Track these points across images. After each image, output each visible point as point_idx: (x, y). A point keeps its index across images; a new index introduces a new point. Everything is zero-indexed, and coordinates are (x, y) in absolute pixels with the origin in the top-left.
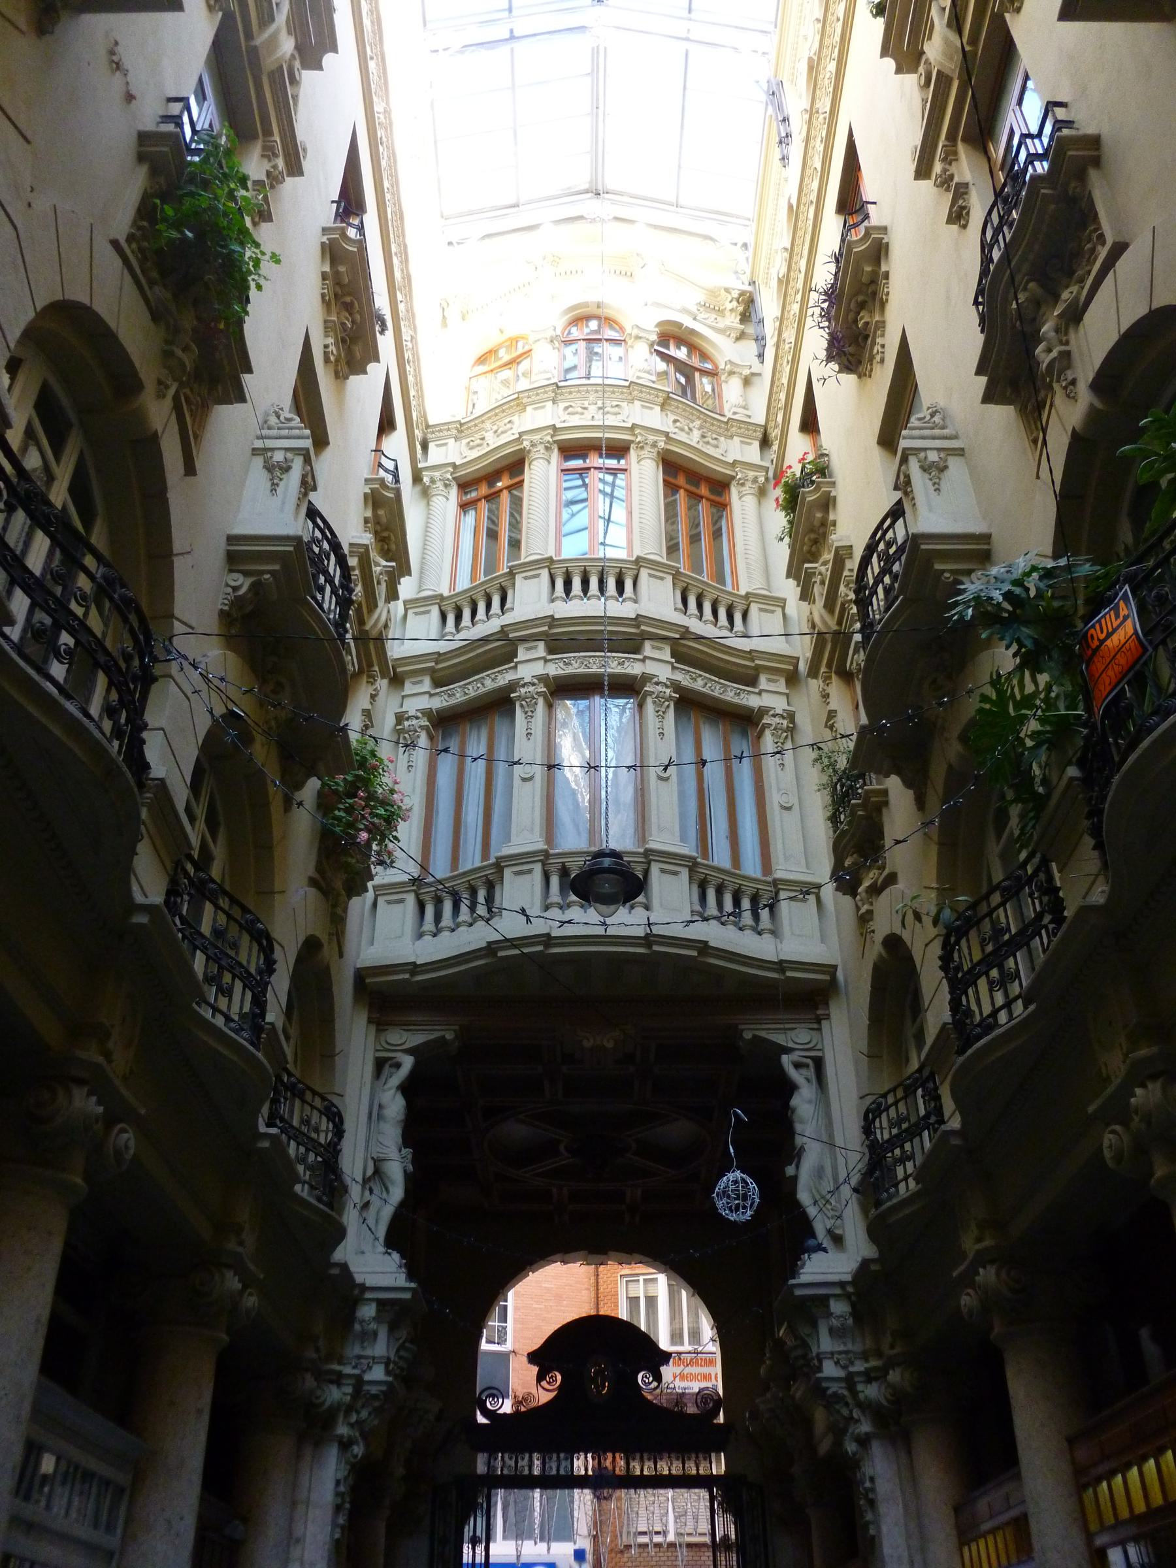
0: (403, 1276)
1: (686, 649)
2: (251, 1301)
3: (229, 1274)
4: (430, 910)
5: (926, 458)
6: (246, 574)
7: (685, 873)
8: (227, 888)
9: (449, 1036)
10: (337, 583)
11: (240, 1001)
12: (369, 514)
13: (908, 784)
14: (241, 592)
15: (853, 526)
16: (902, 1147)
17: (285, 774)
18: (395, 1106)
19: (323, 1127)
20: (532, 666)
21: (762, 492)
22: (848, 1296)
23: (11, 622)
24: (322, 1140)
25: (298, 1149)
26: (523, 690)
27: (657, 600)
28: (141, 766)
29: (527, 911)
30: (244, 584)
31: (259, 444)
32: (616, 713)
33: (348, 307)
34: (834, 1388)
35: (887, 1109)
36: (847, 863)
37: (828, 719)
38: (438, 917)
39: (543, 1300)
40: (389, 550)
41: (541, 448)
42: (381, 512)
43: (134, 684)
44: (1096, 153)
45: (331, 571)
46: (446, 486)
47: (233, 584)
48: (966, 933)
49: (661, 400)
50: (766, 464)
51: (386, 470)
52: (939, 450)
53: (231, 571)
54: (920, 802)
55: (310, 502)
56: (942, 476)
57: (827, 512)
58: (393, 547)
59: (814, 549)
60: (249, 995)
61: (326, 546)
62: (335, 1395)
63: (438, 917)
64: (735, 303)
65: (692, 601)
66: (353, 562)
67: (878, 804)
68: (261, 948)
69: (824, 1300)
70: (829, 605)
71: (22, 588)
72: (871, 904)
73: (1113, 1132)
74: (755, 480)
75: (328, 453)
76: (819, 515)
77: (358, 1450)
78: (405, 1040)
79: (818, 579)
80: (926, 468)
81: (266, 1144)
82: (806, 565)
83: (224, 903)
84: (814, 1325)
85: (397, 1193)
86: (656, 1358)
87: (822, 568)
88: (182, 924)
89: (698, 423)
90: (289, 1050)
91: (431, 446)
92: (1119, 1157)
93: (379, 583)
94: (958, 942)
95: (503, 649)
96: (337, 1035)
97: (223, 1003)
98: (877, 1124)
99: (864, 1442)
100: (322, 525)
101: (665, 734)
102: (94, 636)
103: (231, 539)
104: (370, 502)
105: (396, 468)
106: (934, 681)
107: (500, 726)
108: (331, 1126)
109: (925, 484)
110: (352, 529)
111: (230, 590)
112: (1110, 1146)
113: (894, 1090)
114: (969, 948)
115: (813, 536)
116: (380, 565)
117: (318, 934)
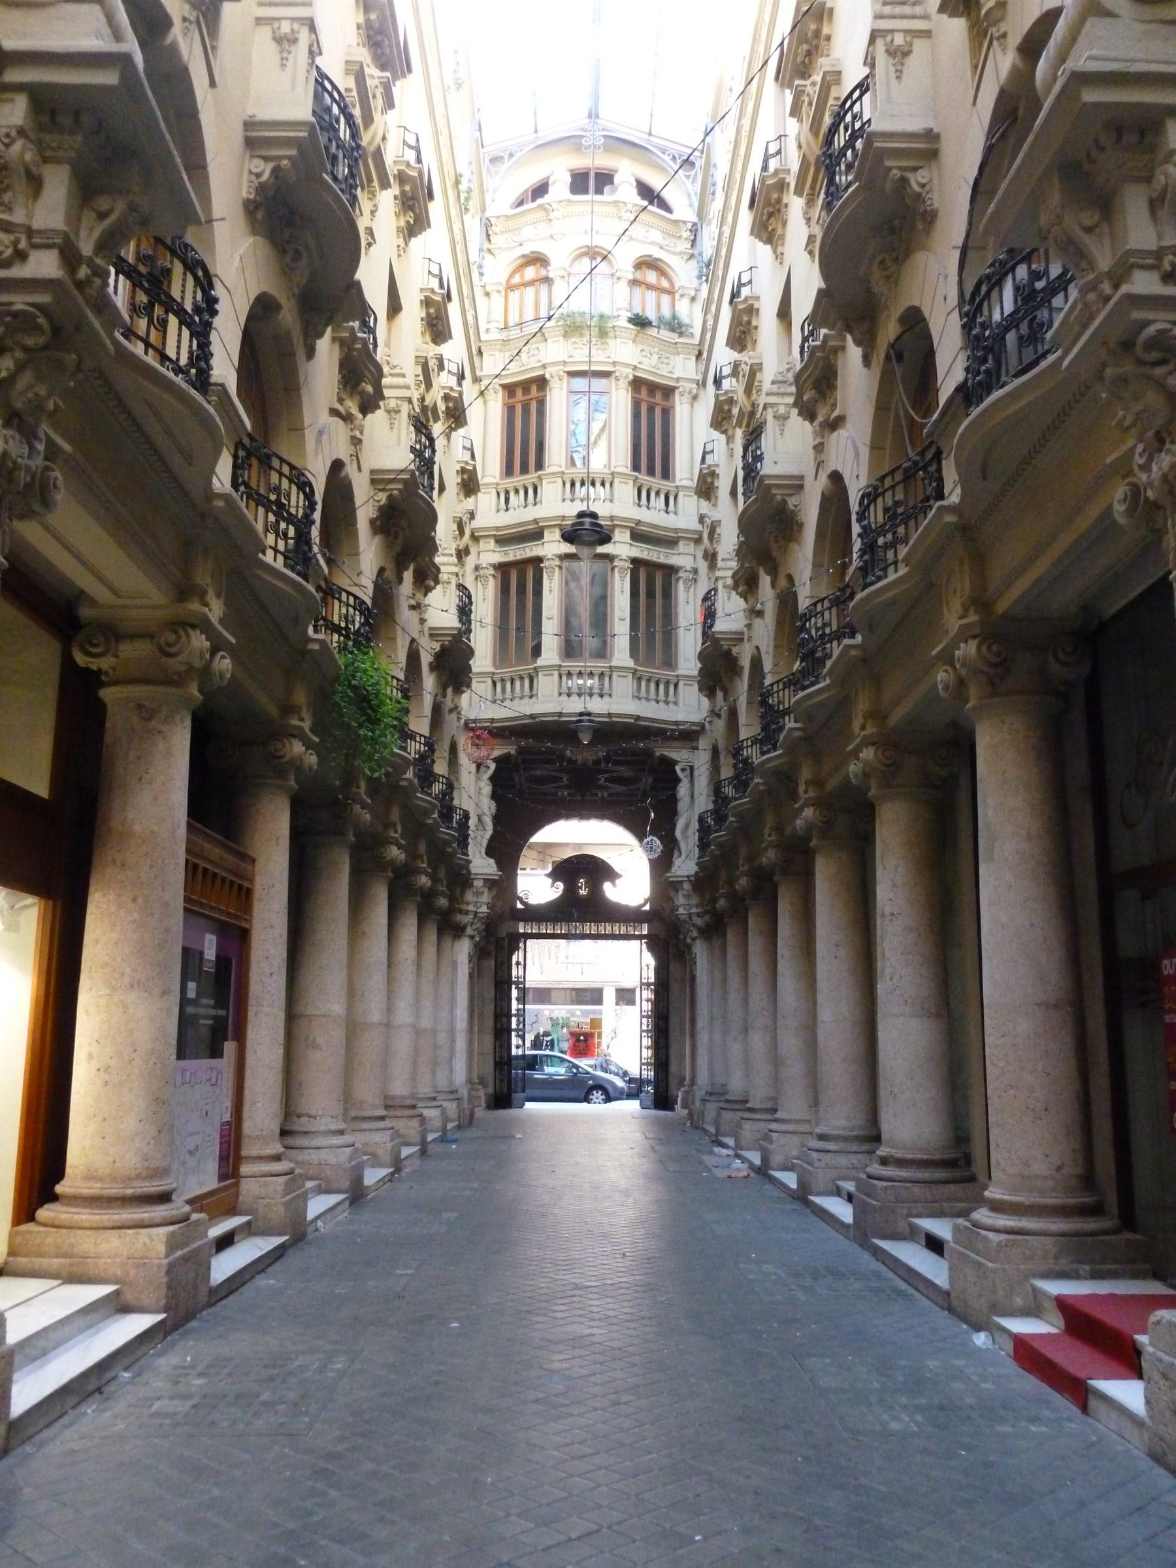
2: (224, 664)
4: (499, 686)
5: (892, 41)
6: (266, 159)
9: (513, 752)
18: (487, 789)
22: (690, 881)
30: (383, 497)
34: (683, 917)
35: (883, 493)
36: (805, 398)
37: (807, 246)
38: (504, 690)
42: (373, 16)
47: (255, 170)
48: (875, 500)
55: (317, 67)
56: (905, 60)
58: (388, 51)
63: (504, 690)
69: (682, 882)
72: (823, 437)
73: (946, 671)
74: (690, 392)
80: (891, 52)
81: (316, 647)
84: (677, 891)
92: (946, 688)
93: (374, 97)
94: (869, 505)
95: (535, 534)
99: (694, 939)
103: (249, 125)
106: (882, 262)
109: (887, 69)
111: (253, 178)
113: (893, 472)
114: (875, 511)
117: (273, 292)
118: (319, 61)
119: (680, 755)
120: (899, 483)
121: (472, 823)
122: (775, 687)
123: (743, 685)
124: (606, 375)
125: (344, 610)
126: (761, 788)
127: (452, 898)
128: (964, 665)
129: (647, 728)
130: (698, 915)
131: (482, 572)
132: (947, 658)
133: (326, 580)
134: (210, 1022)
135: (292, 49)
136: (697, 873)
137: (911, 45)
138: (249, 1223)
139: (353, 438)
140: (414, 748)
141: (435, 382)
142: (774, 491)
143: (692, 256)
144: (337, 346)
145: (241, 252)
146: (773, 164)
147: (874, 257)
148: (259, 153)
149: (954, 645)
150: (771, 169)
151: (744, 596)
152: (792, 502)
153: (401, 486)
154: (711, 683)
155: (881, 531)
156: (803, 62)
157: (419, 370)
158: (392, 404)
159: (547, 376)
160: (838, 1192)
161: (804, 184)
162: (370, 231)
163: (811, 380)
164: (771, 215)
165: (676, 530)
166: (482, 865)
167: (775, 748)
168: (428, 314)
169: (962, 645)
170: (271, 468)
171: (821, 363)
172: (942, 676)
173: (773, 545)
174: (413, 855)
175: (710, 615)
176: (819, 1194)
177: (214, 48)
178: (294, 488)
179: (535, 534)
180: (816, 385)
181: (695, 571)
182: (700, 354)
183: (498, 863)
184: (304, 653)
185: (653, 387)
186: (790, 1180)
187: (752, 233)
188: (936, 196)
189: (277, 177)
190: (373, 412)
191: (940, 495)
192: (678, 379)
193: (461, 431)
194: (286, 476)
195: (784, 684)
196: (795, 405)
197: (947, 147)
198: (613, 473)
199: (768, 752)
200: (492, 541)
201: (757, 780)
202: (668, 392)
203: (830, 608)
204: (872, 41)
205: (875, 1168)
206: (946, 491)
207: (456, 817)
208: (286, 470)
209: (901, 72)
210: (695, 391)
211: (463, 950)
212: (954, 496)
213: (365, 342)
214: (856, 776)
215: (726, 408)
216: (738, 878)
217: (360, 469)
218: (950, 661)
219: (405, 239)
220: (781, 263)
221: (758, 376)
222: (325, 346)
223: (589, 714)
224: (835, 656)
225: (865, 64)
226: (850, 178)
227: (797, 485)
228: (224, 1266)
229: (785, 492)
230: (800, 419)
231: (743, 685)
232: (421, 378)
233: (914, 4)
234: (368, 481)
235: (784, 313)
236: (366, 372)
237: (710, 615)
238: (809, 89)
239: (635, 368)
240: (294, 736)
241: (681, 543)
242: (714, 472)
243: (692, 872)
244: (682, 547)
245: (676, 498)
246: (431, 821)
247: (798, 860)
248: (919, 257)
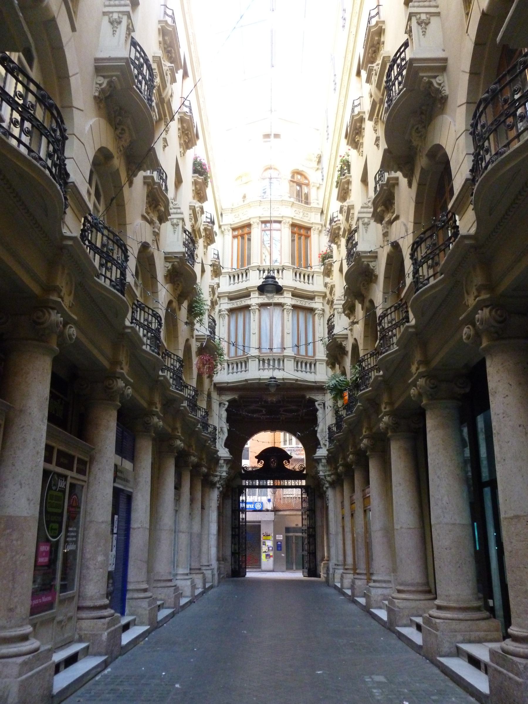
3: (53, 313)
4: (230, 366)
7: (293, 360)
8: (106, 225)
9: (236, 397)
10: (147, 78)
11: (115, 274)
12: (161, 39)
13: (405, 176)
14: (103, 86)
15: (390, 46)
16: (392, 331)
17: (128, 170)
18: (224, 414)
19: (154, 321)
21: (320, 232)
23: (3, 121)
24: (153, 327)
25: (143, 331)
28: (63, 175)
29: (254, 372)
30: (169, 265)
31: (107, 9)
32: (277, 312)
33: (187, 135)
34: (322, 477)
35: (387, 316)
37: (376, 142)
38: (233, 369)
39: (259, 442)
40: (171, 57)
41: (256, 224)
42: (197, 186)
43: (59, 142)
44: (445, 64)
50: (321, 223)
52: (427, 13)
53: (98, 76)
54: (410, 185)
55: (132, 38)
56: (427, 27)
57: (381, 37)
58: (174, 55)
59: (374, 56)
60: (119, 271)
61: (142, 60)
62: (217, 479)
63: (233, 369)
65: (298, 275)
66: (154, 66)
67: (393, 184)
69: (321, 459)
70: (378, 86)
71: (6, 102)
73: (468, 328)
74: (318, 229)
75: (140, 8)
76: (377, 38)
77: (221, 489)
78: (226, 398)
79: (374, 72)
80: (364, 224)
82: (369, 65)
83: (106, 232)
84: (318, 464)
85: (226, 435)
86: (288, 457)
87: (376, 66)
88: (89, 243)
89: (302, 210)
90: (138, 294)
91: (223, 215)
92: (468, 338)
93: (167, 75)
94: (417, 248)
95: (246, 295)
96: (127, 216)
97: (108, 274)
98: (383, 321)
99: (327, 488)
101: (289, 317)
102: (40, 122)
103: (97, 60)
104: (161, 33)
105: (173, 14)
106: (364, 284)
107: (247, 313)
108: (157, 321)
110: (152, 47)
111: (98, 86)
112: (466, 333)
113: (390, 308)
115: (373, 49)
116: (167, 65)
118: (133, 34)
119: (318, 397)
122: (366, 356)
123: (348, 361)
124: (280, 222)
126: (361, 408)
127: (209, 469)
128: (482, 324)
129: (301, 385)
130: (329, 475)
131: (222, 313)
132: (470, 321)
133: (166, 350)
135: (119, 26)
136: (328, 455)
137: (430, 19)
138: (87, 648)
139: (154, 232)
140: (200, 414)
141: (199, 219)
142: (337, 340)
143: (318, 169)
144: (146, 187)
145: (91, 123)
146: (357, 110)
147: (413, 127)
148: (100, 74)
149: (416, 380)
150: (356, 112)
151: (348, 316)
152: (372, 265)
153: (178, 260)
154: (333, 361)
156: (372, 57)
157: (191, 212)
158: (175, 221)
159: (252, 223)
160: (411, 623)
161: (374, 115)
162: (197, 255)
163: (381, 202)
164: (336, 237)
165: (313, 292)
166: (224, 453)
167: (367, 387)
168: (196, 188)
169: (480, 311)
170: (171, 358)
171: (387, 192)
172: (466, 331)
173: (362, 288)
174: (201, 459)
175: (331, 328)
176: (358, 597)
177: (159, 240)
178: (154, 319)
179: (246, 295)
180: (384, 204)
181: (323, 310)
182: (322, 212)
183: (231, 452)
184: (157, 381)
185: (300, 227)
186: (383, 614)
187: (338, 199)
188: (446, 88)
189: (111, 87)
190: (164, 222)
191: (408, 321)
193: (212, 246)
195: (371, 355)
196: (373, 216)
197: (379, 256)
199: (349, 415)
200: (227, 299)
201: (359, 404)
202: (309, 229)
203: (395, 311)
204: (410, 19)
205: (434, 612)
206: (410, 320)
207: (210, 429)
208: (150, 312)
209: (425, 32)
210: (320, 229)
211: (215, 495)
212: (413, 322)
213: (160, 185)
214: (414, 396)
215: (337, 232)
216: (339, 467)
217: (158, 249)
218: (415, 386)
219: (183, 149)
220: (362, 156)
221: (352, 212)
222: (185, 304)
223: (275, 378)
224: (442, 263)
225: (406, 33)
226: (400, 87)
227: (374, 256)
228: (126, 638)
229: (369, 260)
230: (375, 223)
231: (348, 361)
232: (192, 215)
233: (430, 1)
234: (163, 258)
235: (364, 180)
236: (160, 200)
237: (331, 328)
238: (376, 68)
239: (292, 218)
240: (177, 438)
241: (316, 298)
242: (349, 180)
243: (326, 455)
244: (317, 299)
245: (313, 277)
246: (197, 429)
247: (381, 447)
248: (440, 118)
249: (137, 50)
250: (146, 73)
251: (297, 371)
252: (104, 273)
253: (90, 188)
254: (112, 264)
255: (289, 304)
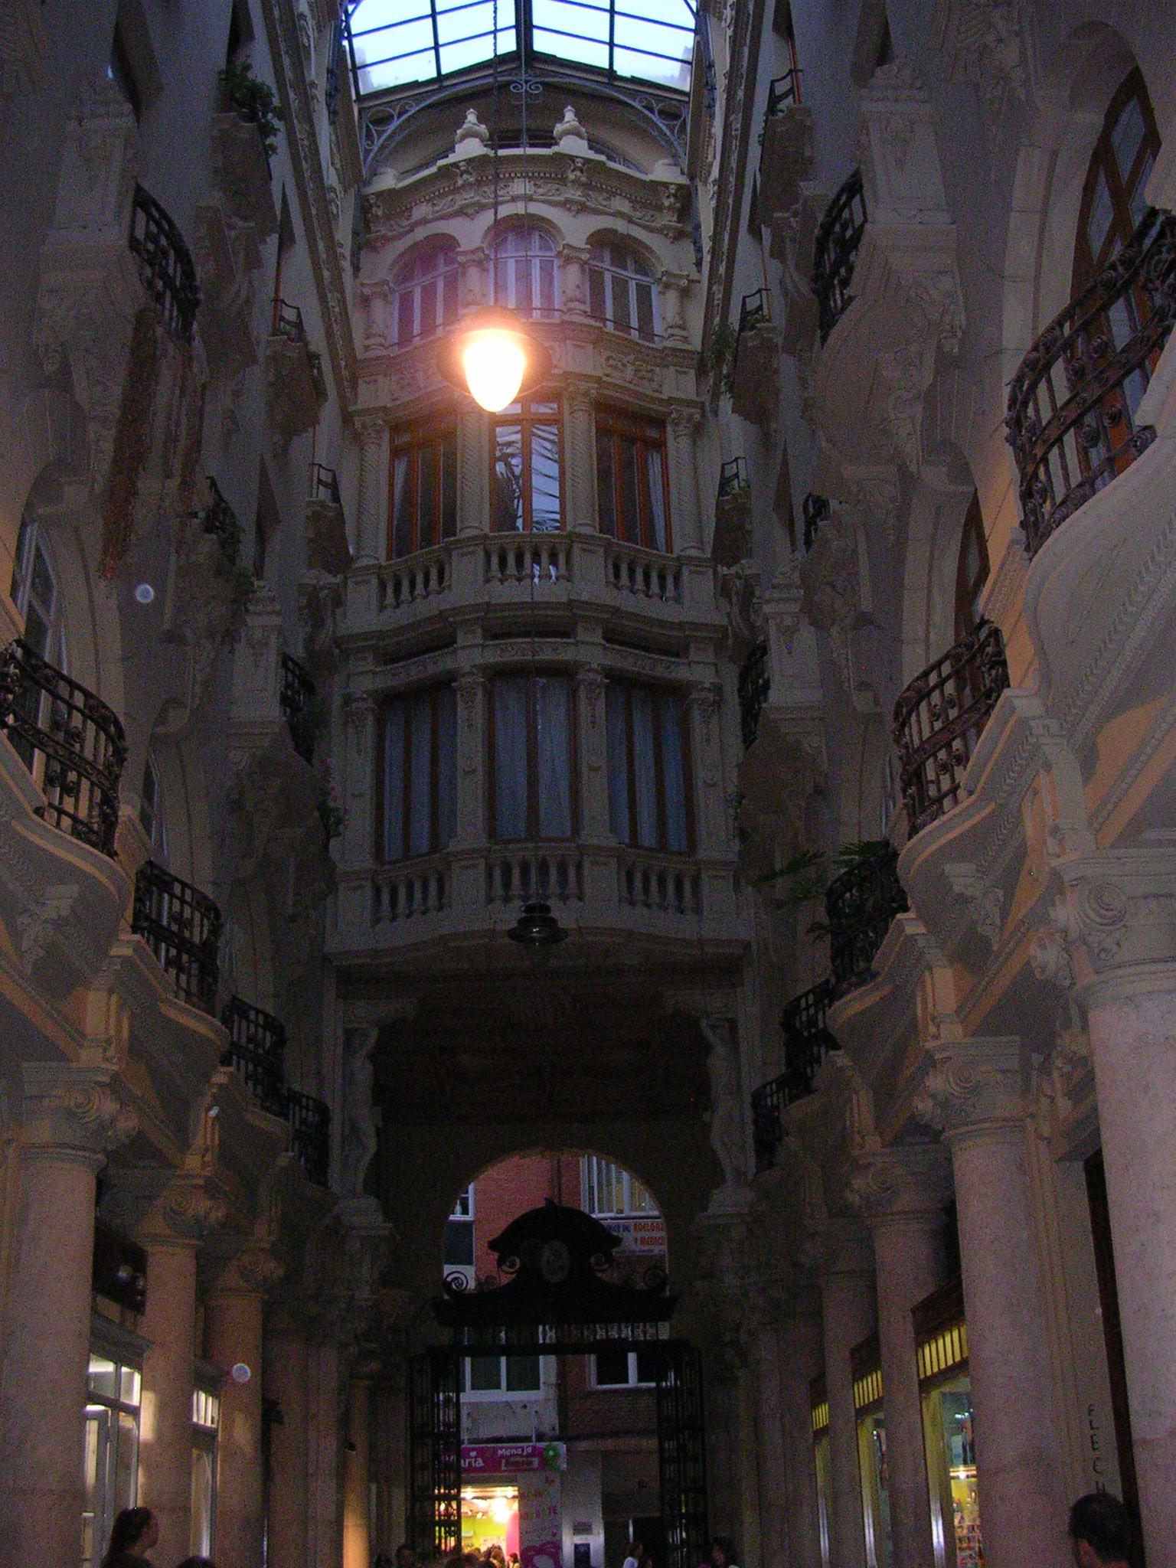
0: (380, 1218)
1: (619, 633)
18: (363, 1070)
20: (471, 655)
26: (463, 681)
27: (591, 582)
45: (171, 271)
46: (378, 432)
49: (593, 337)
51: (288, 322)
61: (164, 241)
64: (672, 200)
68: (110, 738)
74: (690, 418)
95: (440, 637)
97: (69, 804)
100: (157, 215)
105: (299, 315)
114: (919, 722)
120: (948, 677)
121: (335, 1130)
125: (252, 1029)
134: (367, 1383)
155: (928, 749)
165: (681, 625)
170: (249, 1021)
178: (91, 726)
179: (442, 640)
181: (718, 689)
192: (670, 401)
194: (78, 710)
198: (569, 536)
202: (660, 423)
208: (79, 699)
249: (150, 217)
250: (175, 270)
251: (632, 903)
252: (56, 803)
253: (40, 610)
254: (80, 775)
255: (595, 666)
